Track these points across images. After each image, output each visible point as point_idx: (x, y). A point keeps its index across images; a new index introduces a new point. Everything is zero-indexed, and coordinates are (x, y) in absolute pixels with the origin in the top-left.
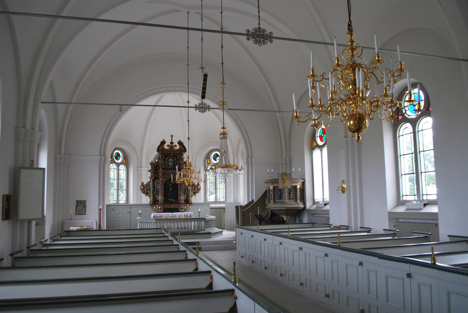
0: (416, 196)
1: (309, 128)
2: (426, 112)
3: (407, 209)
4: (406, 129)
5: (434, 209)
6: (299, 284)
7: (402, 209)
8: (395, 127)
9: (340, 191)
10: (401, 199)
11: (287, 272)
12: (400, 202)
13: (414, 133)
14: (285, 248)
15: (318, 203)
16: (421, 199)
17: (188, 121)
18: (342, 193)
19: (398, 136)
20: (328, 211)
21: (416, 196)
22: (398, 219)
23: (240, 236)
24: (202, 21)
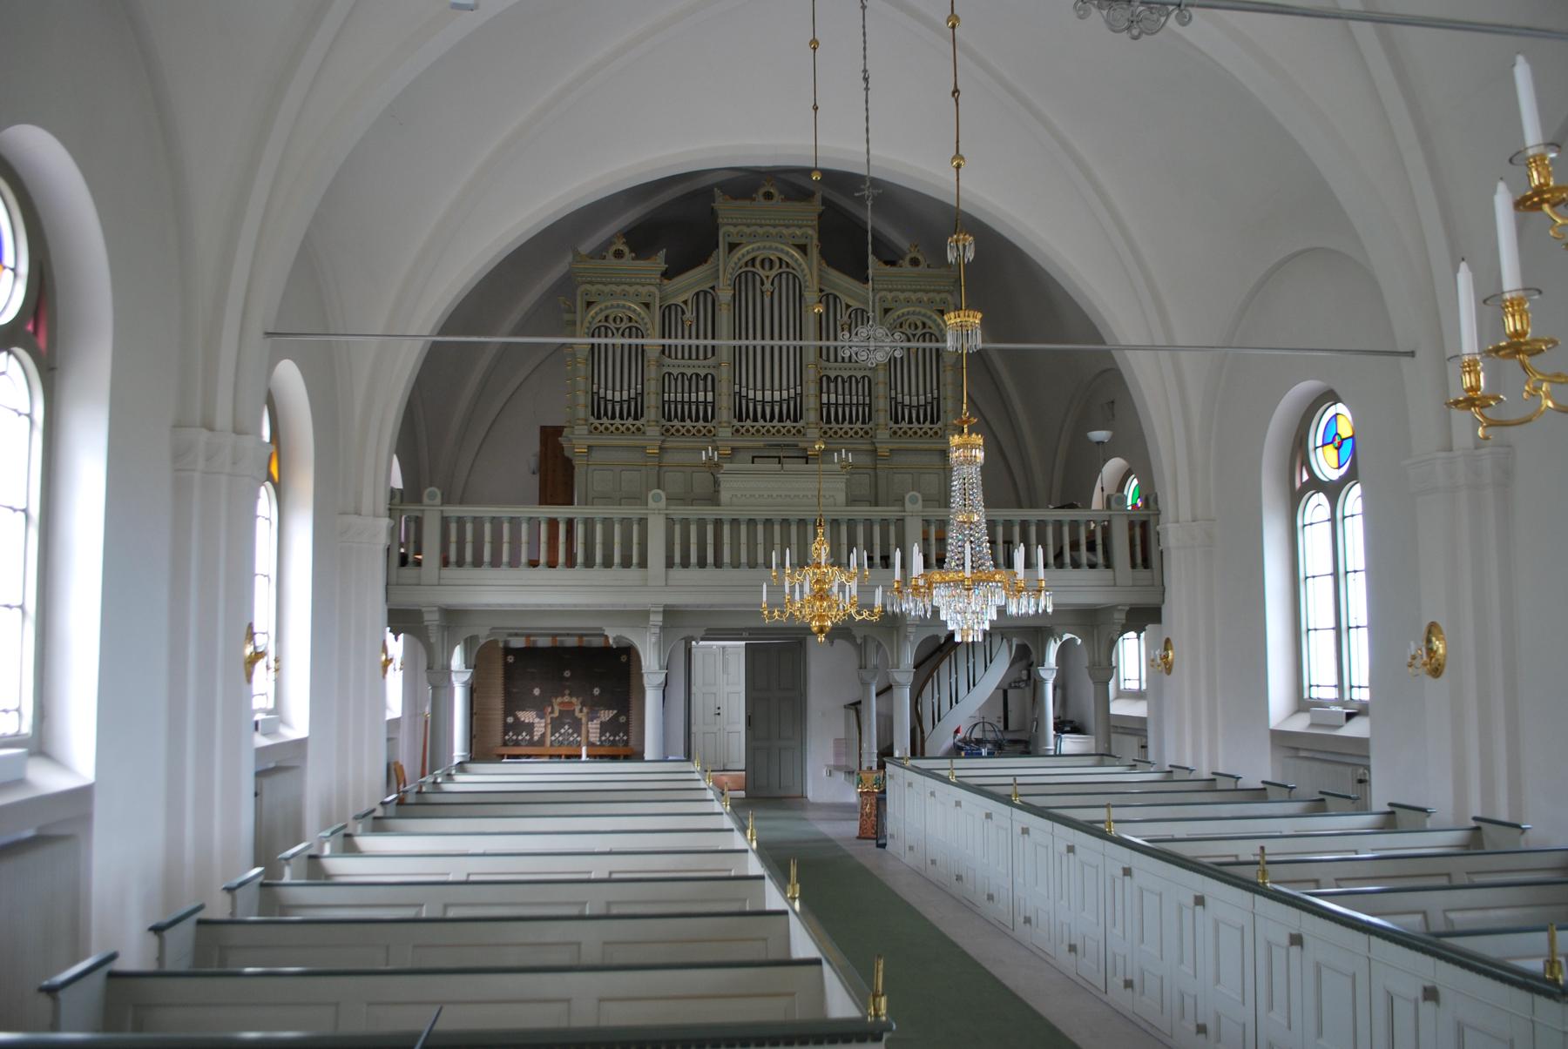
0: (1332, 694)
1: (1306, 387)
2: (1351, 476)
3: (1312, 725)
4: (1316, 507)
5: (1358, 729)
6: (1193, 1028)
7: (1300, 724)
8: (1295, 500)
9: (1422, 671)
10: (1306, 696)
11: (1189, 1002)
12: (1302, 703)
13: (1333, 520)
14: (1460, 1029)
15: (1320, 703)
16: (1347, 697)
17: (956, 91)
18: (1429, 680)
19: (1299, 524)
20: (1360, 746)
21: (1332, 694)
22: (1297, 749)
23: (1187, 913)
24: (865, 71)
